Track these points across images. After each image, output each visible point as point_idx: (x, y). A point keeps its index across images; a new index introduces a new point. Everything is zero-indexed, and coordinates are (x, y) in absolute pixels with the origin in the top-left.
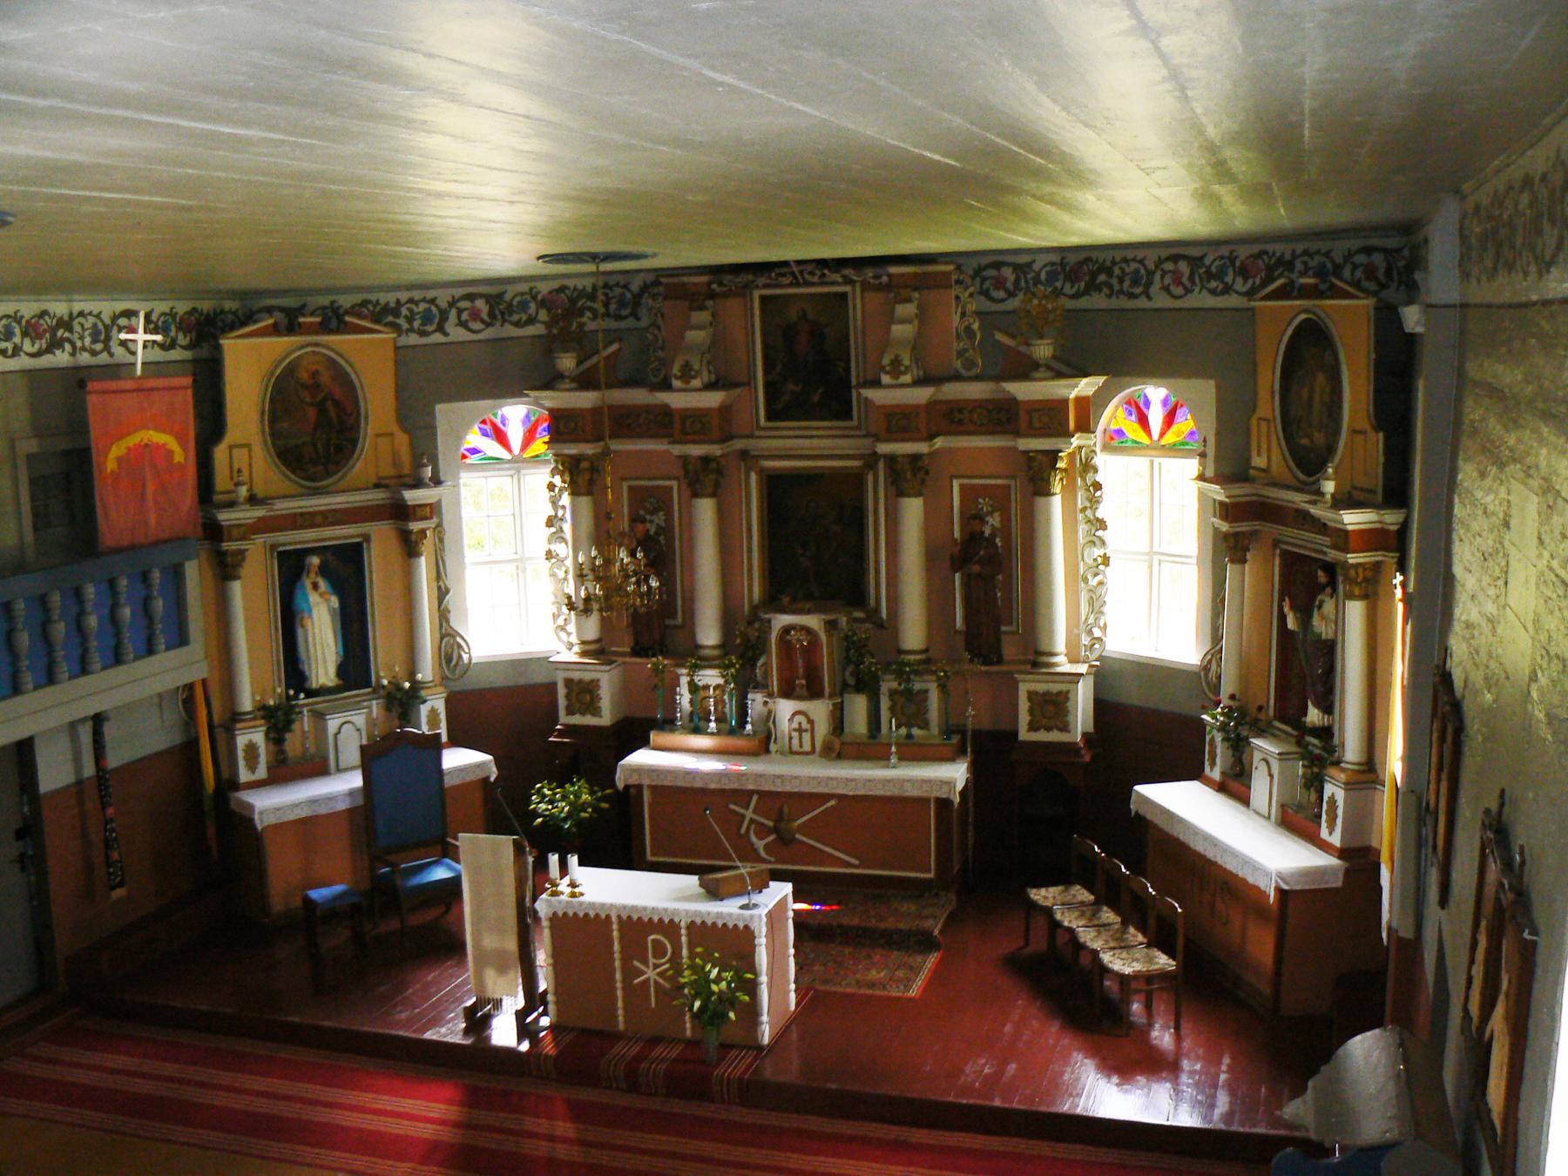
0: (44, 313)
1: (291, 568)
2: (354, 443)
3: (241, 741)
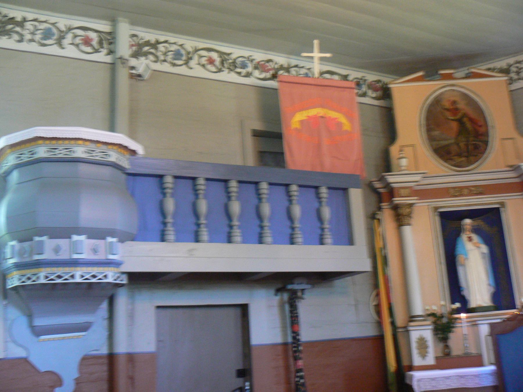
0: (270, 61)
1: (451, 224)
2: (486, 143)
3: (415, 335)
